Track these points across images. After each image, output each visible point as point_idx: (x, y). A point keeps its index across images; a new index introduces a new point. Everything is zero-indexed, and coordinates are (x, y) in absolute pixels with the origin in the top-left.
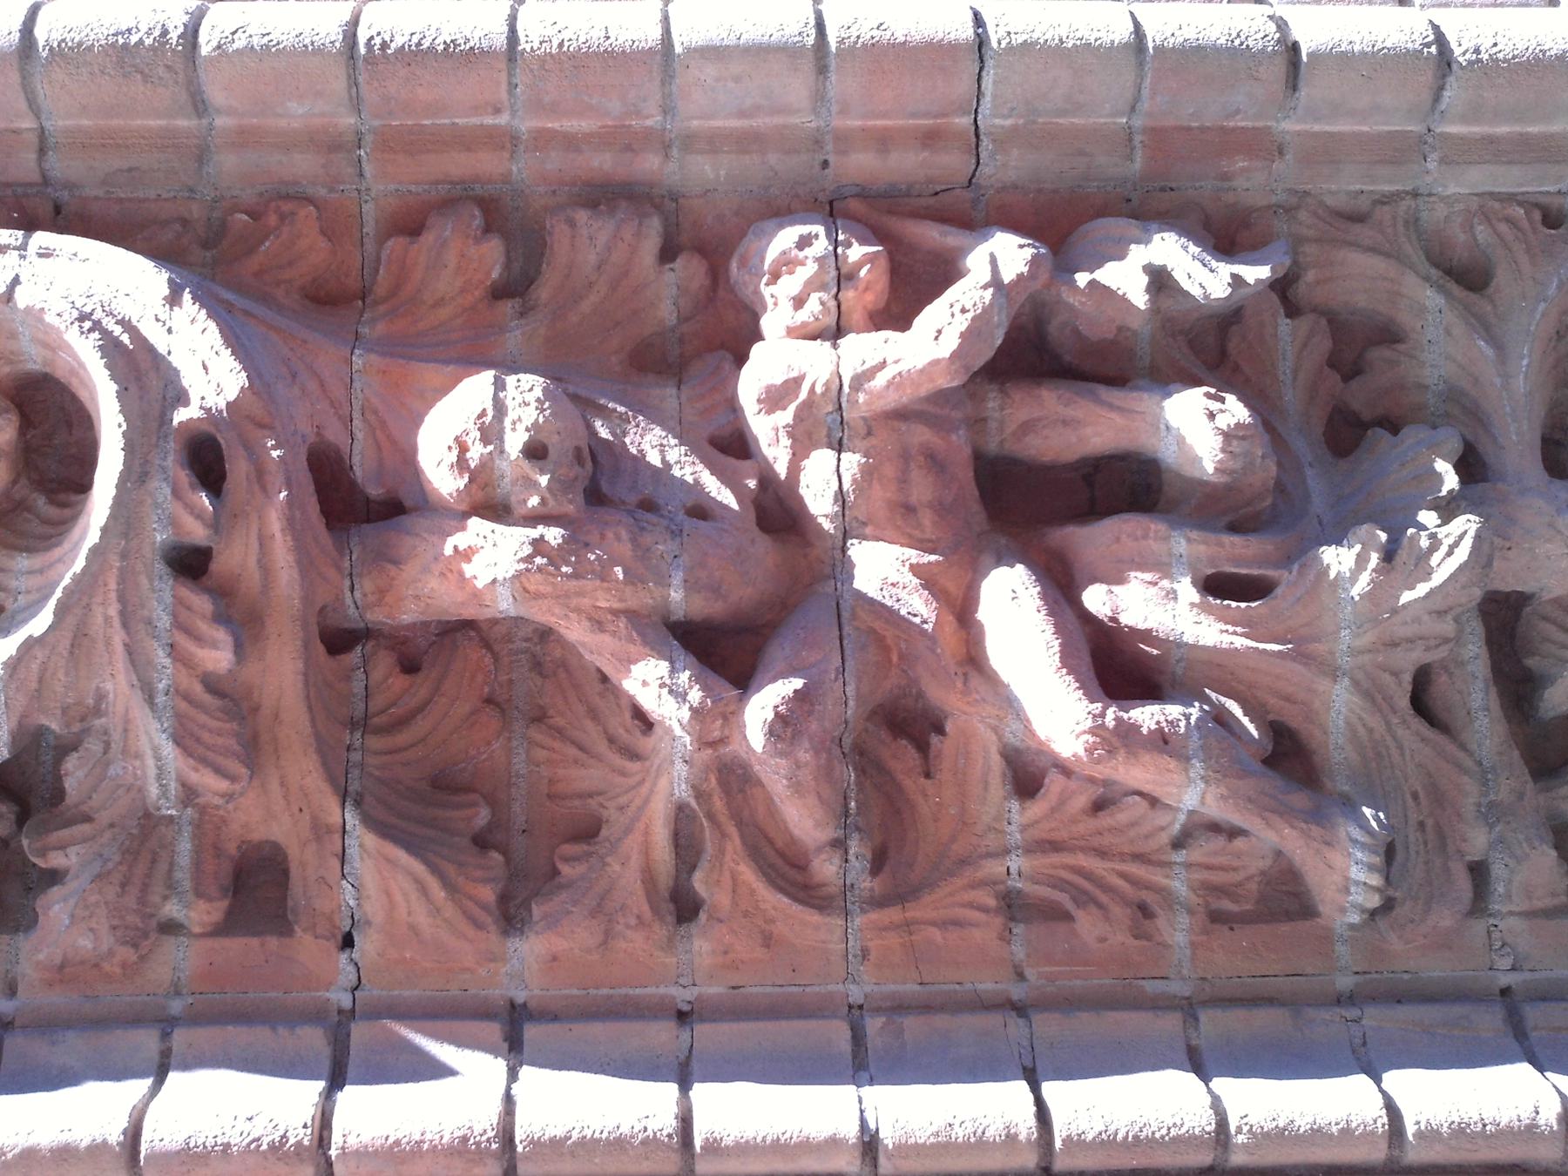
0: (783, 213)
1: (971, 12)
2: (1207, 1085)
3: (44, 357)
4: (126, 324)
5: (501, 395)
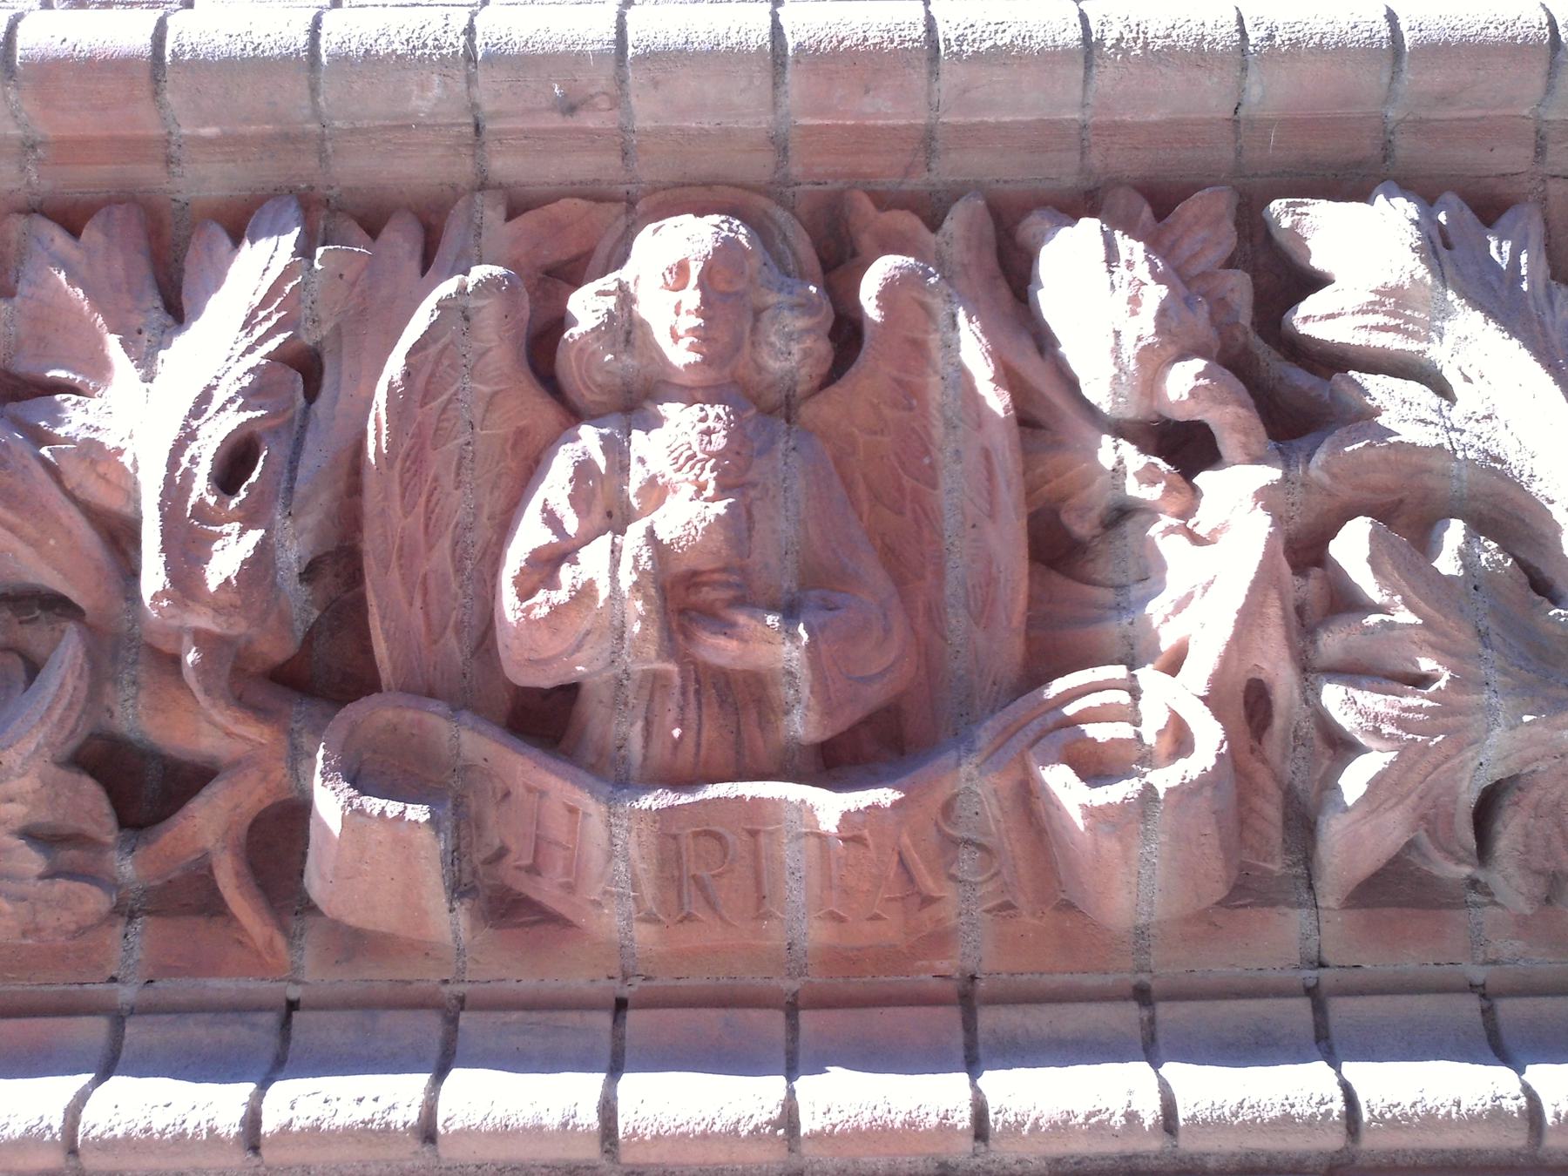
0: (1071, 209)
1: (1385, 9)
2: (1157, 1072)
3: (689, 349)
4: (249, 324)
5: (228, 405)
